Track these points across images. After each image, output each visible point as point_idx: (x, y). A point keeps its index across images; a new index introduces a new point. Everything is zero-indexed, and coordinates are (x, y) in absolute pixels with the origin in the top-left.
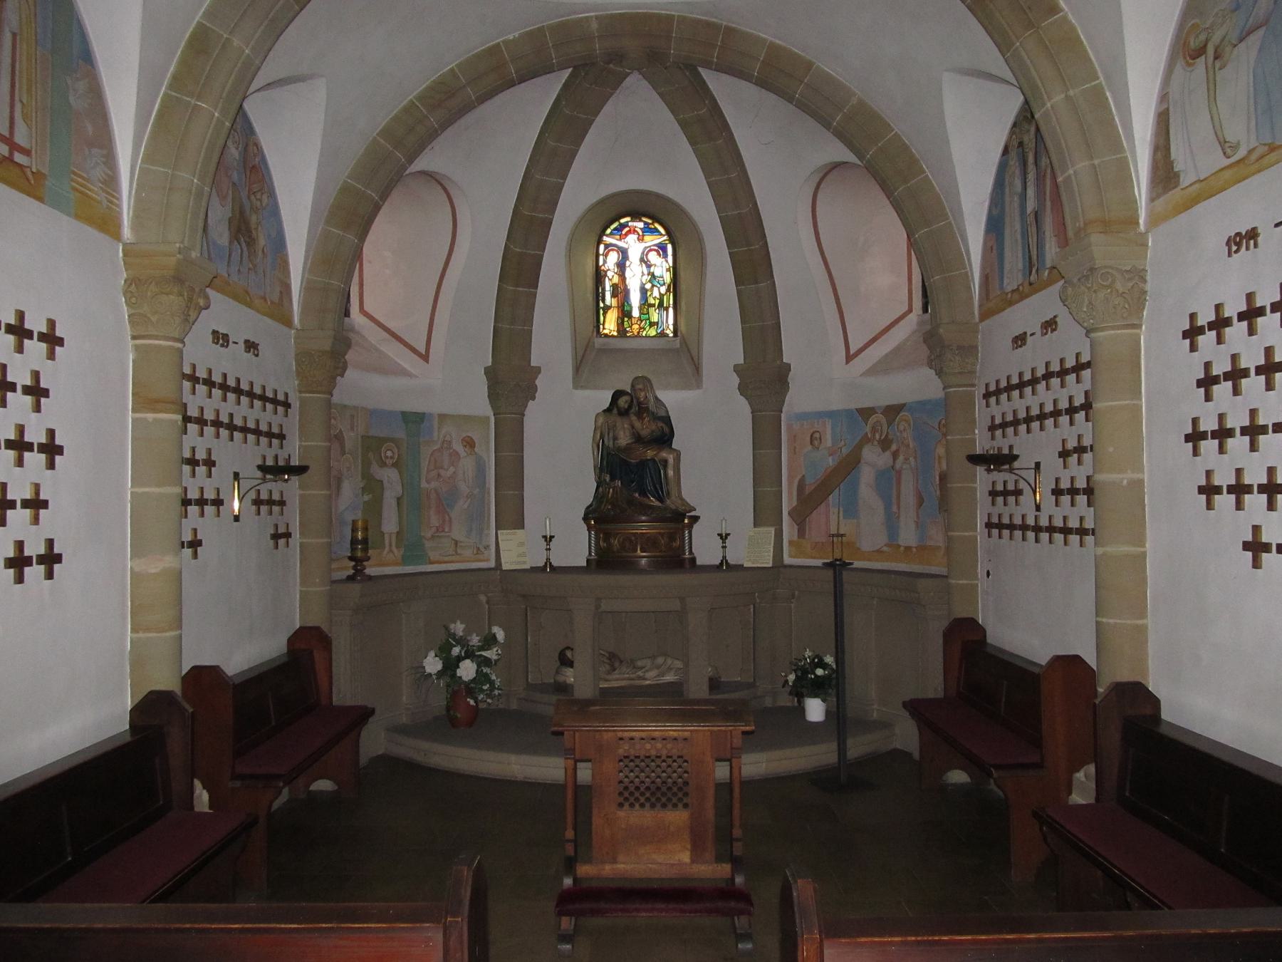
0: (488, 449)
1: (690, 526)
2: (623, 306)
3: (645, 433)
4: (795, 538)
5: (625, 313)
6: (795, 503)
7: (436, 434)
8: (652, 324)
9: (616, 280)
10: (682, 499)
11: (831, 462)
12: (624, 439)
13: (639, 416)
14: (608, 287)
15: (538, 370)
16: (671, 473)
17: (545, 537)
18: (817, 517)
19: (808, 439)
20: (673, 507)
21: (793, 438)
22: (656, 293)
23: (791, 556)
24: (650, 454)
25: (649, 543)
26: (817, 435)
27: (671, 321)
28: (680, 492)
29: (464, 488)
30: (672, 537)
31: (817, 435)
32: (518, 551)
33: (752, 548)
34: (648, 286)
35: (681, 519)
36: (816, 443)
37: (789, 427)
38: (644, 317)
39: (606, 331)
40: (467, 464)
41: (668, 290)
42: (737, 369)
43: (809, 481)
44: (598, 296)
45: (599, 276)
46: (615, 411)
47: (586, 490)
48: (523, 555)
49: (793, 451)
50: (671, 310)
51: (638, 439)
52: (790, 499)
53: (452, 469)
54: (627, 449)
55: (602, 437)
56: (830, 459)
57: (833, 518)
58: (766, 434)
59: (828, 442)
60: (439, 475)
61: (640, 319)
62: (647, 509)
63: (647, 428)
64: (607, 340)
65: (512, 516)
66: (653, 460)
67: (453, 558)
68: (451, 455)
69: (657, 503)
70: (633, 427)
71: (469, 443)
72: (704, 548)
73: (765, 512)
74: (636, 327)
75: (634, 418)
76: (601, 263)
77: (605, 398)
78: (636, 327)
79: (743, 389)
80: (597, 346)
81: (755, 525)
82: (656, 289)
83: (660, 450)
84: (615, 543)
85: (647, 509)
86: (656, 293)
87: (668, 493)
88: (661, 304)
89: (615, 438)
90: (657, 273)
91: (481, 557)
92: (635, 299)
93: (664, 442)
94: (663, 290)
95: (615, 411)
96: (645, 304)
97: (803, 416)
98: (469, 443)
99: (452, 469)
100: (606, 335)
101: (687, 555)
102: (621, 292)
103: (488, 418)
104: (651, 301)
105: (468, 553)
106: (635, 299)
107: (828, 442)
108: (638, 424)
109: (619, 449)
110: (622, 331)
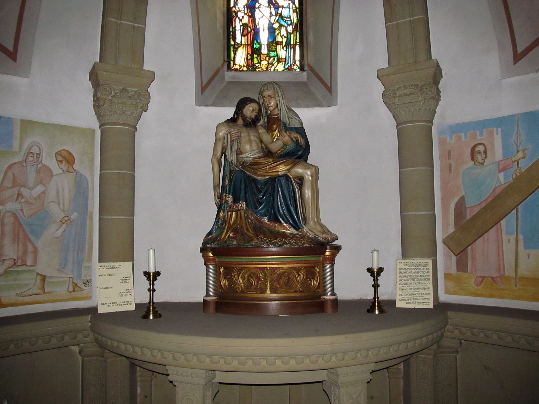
0: (92, 169)
1: (332, 260)
2: (252, 43)
3: (276, 147)
4: (453, 270)
5: (255, 51)
6: (452, 229)
7: (16, 143)
8: (279, 61)
9: (246, 20)
10: (322, 226)
11: (502, 179)
12: (250, 152)
13: (269, 128)
14: (238, 27)
15: (151, 77)
16: (308, 193)
17: (147, 274)
18: (483, 249)
19: (468, 151)
20: (311, 235)
21: (448, 155)
22: (283, 32)
23: (447, 292)
24: (282, 169)
25: (282, 281)
26: (481, 148)
27: (298, 57)
28: (318, 217)
29: (56, 211)
30: (310, 273)
31: (481, 148)
32: (114, 290)
33: (411, 287)
34: (276, 26)
35: (322, 249)
36: (479, 158)
37: (442, 142)
38: (272, 54)
39: (237, 67)
40: (62, 184)
41: (295, 30)
42: (381, 75)
43: (469, 203)
44: (230, 34)
45: (230, 16)
46: (240, 122)
47: (206, 217)
48: (128, 293)
49: (448, 169)
50: (298, 48)
51: (268, 153)
52: (445, 224)
53: (40, 189)
54: (254, 164)
55: (223, 153)
56: (501, 176)
57: (508, 248)
58: (414, 148)
59: (498, 153)
60: (19, 194)
61: (268, 55)
62: (276, 237)
63: (278, 141)
64: (236, 73)
65: (119, 246)
66: (286, 177)
67: (37, 298)
68: (38, 171)
69: (292, 231)
70: (261, 141)
71: (67, 159)
72: (347, 281)
73: (415, 240)
74: (264, 63)
75: (262, 131)
76: (232, 5)
77: (229, 112)
78: (264, 63)
79: (388, 98)
80: (227, 78)
81: (405, 255)
82: (283, 29)
83: (295, 164)
84: (240, 281)
85: (276, 237)
86: (283, 32)
87: (305, 219)
88: (288, 44)
89: (240, 152)
90: (285, 13)
91: (78, 294)
92: (264, 37)
93: (300, 157)
94: (290, 29)
95: (240, 122)
96: (273, 44)
97: (458, 129)
98: (67, 159)
99: (40, 189)
100: (236, 70)
101: (329, 297)
102: (252, 31)
103: (93, 131)
104: (279, 39)
105: (62, 290)
106: (264, 37)
107: (498, 153)
108: (266, 137)
109: (243, 164)
110: (251, 67)
